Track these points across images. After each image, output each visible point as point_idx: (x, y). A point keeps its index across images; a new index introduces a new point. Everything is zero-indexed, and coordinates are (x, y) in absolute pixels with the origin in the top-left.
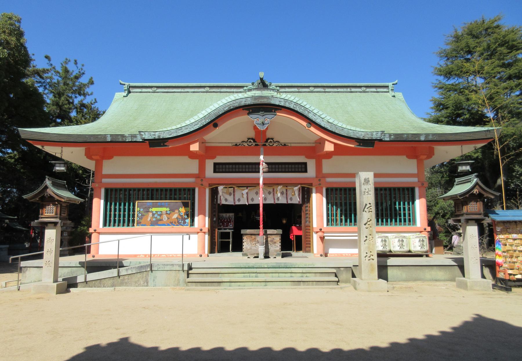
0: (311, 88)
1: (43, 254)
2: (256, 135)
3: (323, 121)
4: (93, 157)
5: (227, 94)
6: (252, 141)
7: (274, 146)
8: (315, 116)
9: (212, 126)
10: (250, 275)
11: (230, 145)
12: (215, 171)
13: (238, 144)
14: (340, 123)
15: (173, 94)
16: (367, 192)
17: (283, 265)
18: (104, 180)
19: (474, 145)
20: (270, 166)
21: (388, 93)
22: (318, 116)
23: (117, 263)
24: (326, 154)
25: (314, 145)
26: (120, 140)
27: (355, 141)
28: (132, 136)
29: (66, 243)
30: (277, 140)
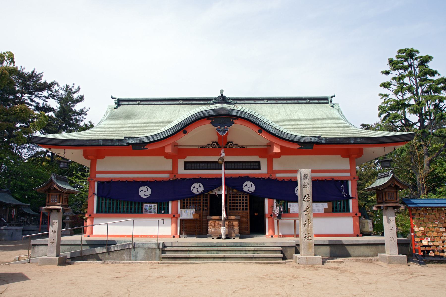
0: (265, 100)
1: (48, 234)
2: (218, 139)
3: (271, 128)
4: (89, 157)
5: (197, 105)
6: (215, 144)
8: (265, 124)
9: (182, 133)
11: (197, 147)
12: (185, 169)
13: (204, 147)
14: (285, 130)
15: (153, 106)
16: (306, 185)
17: (239, 245)
18: (98, 176)
20: (228, 164)
23: (106, 242)
24: (275, 154)
25: (266, 147)
26: (110, 144)
27: (298, 144)
29: (69, 225)
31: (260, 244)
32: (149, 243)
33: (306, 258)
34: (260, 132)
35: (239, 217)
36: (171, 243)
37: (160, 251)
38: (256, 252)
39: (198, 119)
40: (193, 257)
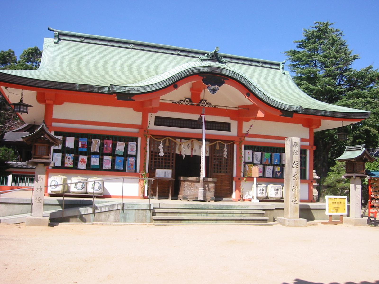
3: (260, 93)
6: (189, 100)
7: (206, 106)
10: (88, 212)
11: (171, 102)
16: (296, 153)
18: (54, 124)
19: (351, 122)
21: (279, 70)
22: (257, 89)
25: (237, 109)
26: (88, 90)
28: (99, 88)
30: (209, 102)
31: (244, 207)
32: (140, 204)
33: (295, 220)
34: (248, 95)
35: (215, 180)
36: (158, 205)
37: (151, 212)
38: (242, 215)
39: (192, 74)
40: (187, 219)
